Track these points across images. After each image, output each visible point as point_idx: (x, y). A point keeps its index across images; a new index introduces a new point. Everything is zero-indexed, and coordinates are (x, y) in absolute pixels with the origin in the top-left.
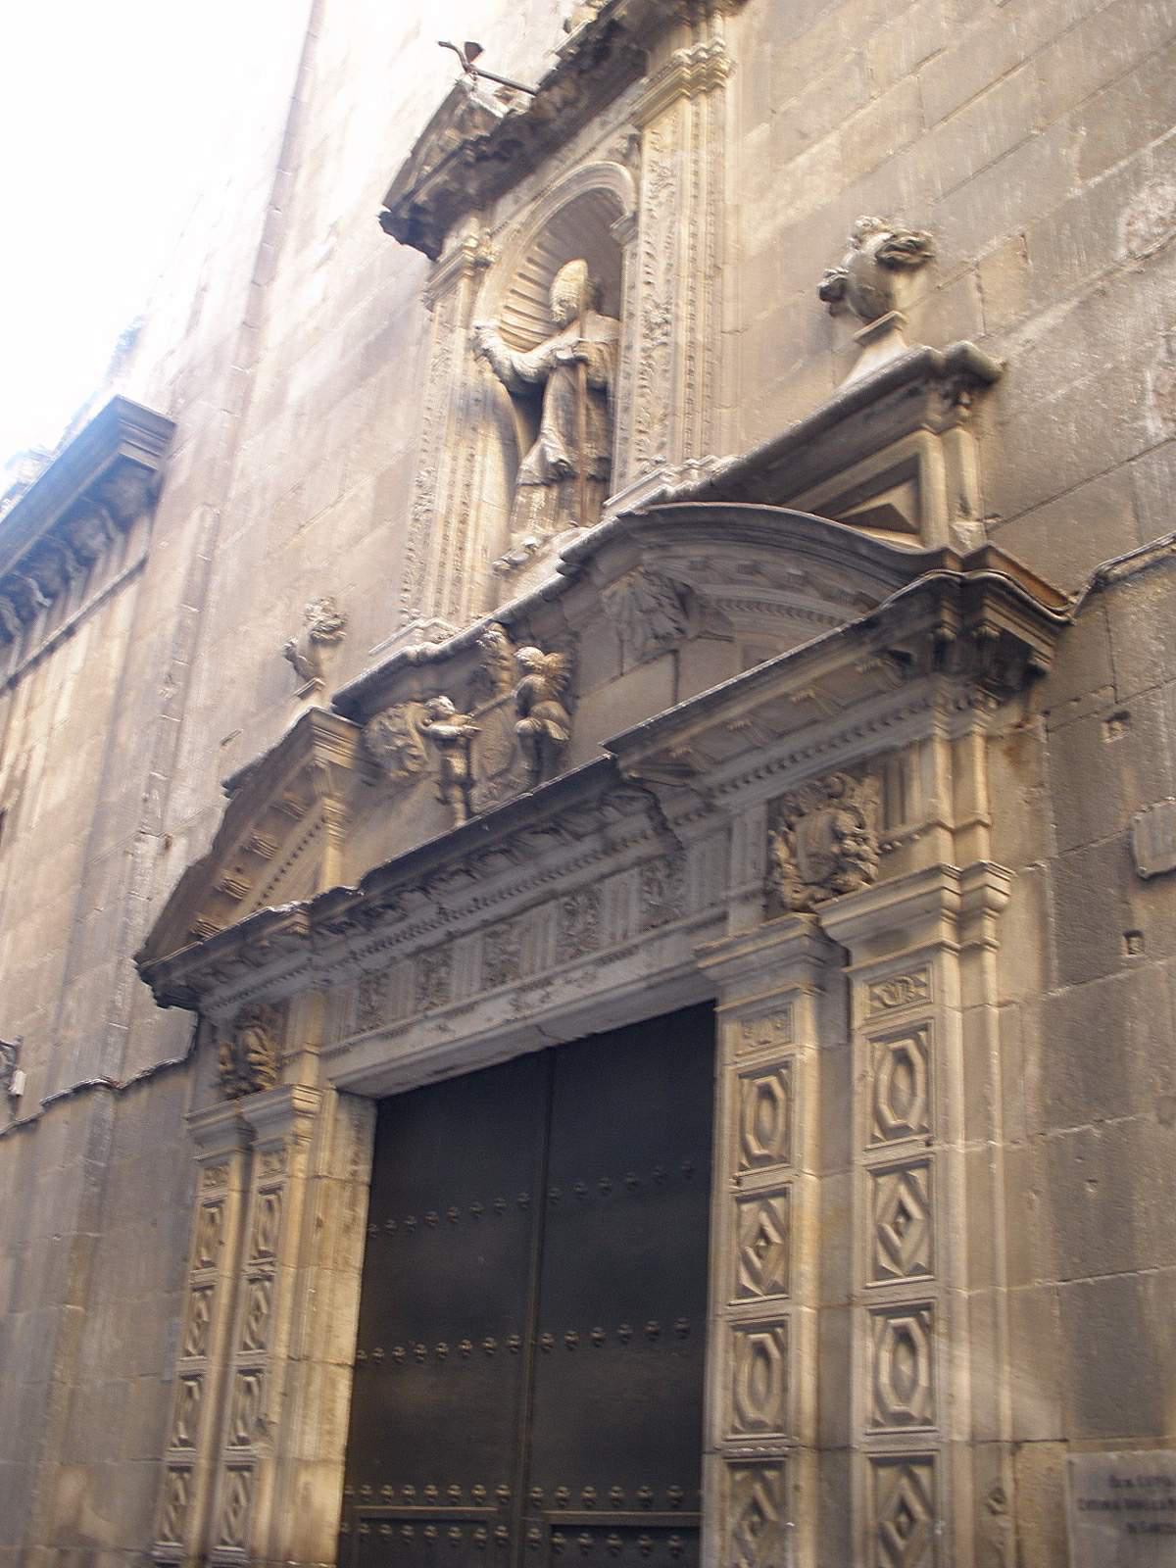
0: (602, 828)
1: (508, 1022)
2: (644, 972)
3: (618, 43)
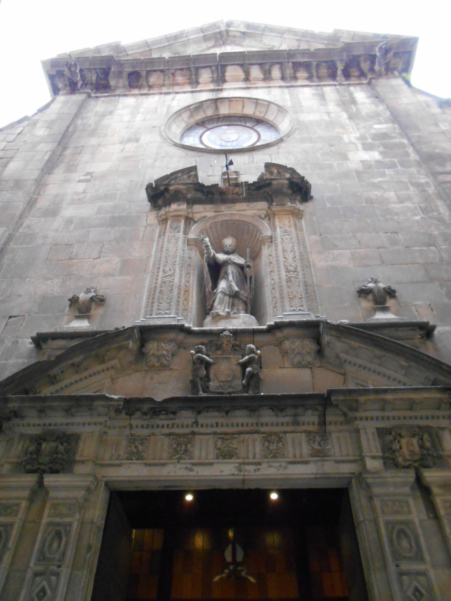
0: (296, 415)
1: (233, 474)
2: (315, 471)
3: (267, 189)
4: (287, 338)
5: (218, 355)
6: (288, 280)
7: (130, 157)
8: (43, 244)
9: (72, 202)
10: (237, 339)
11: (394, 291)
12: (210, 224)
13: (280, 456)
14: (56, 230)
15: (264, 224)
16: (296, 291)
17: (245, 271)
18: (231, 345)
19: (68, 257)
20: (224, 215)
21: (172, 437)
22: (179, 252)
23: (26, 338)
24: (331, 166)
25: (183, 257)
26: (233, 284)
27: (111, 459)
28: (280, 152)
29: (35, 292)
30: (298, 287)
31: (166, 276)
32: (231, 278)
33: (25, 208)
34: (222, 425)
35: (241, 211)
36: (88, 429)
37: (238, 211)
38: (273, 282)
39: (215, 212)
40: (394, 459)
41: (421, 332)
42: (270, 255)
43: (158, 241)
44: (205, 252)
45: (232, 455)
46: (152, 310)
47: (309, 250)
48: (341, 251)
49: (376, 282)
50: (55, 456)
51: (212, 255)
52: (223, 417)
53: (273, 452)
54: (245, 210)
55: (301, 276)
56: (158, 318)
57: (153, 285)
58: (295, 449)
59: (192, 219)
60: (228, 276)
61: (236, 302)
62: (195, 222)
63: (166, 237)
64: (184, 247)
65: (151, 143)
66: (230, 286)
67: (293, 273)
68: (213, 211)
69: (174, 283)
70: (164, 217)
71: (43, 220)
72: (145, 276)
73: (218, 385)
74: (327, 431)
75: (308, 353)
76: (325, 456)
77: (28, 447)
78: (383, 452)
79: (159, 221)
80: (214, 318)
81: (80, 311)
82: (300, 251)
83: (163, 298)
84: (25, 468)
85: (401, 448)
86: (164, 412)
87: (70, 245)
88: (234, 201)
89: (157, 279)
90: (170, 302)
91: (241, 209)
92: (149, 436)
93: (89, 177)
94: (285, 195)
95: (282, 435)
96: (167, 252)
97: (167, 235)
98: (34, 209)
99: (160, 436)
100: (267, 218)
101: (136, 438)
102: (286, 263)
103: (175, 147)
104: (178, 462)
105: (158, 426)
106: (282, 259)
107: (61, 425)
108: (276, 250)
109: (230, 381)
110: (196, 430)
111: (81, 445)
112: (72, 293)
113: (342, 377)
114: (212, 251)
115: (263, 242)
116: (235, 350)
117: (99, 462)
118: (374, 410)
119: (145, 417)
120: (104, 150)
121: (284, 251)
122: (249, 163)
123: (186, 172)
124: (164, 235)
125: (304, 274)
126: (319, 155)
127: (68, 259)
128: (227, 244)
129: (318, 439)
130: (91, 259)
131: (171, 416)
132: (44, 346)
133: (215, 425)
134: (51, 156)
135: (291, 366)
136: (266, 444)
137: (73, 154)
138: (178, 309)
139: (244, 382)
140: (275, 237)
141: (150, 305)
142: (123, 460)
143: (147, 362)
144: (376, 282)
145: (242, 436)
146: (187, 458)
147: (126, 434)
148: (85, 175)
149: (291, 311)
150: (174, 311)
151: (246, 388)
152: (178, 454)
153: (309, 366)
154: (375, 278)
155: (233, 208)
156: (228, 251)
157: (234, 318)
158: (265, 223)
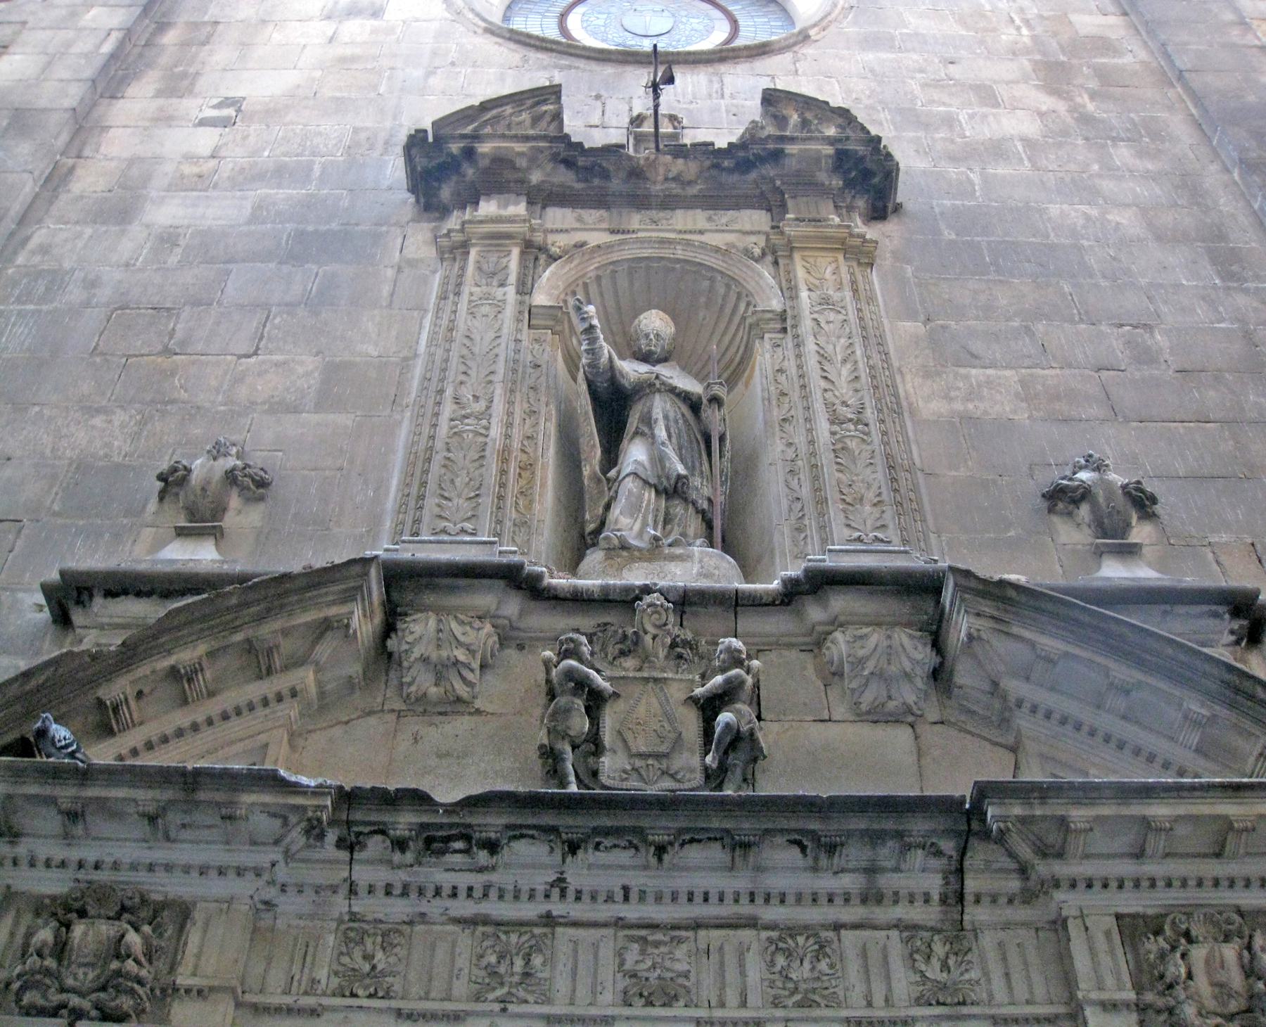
0: (872, 870)
3: (769, 170)
4: (836, 623)
5: (625, 669)
6: (839, 446)
7: (354, 59)
8: (87, 304)
9: (180, 185)
10: (685, 623)
11: (1153, 500)
12: (597, 268)
13: (823, 1003)
14: (127, 265)
15: (761, 276)
16: (863, 481)
17: (703, 415)
18: (668, 640)
19: (160, 347)
20: (638, 240)
21: (481, 929)
22: (503, 346)
23: (25, 591)
24: (949, 121)
25: (515, 361)
26: (670, 452)
27: (287, 992)
28: (800, 72)
29: (53, 450)
30: (869, 470)
31: (466, 417)
32: (661, 432)
33: (37, 196)
34: (642, 896)
35: (690, 232)
36: (218, 887)
37: (680, 232)
38: (790, 454)
39: (613, 232)
40: (1171, 1011)
41: (1236, 625)
42: (780, 371)
43: (438, 309)
44: (583, 348)
45: (673, 993)
46: (417, 521)
47: (896, 364)
48: (990, 372)
49: (1099, 467)
50: (115, 965)
51: (604, 360)
52: (646, 867)
53: (803, 986)
54: (701, 232)
55: (876, 437)
56: (439, 542)
57: (422, 446)
58: (868, 981)
59: (542, 249)
60: (651, 428)
61: (678, 509)
62: (553, 258)
63: (465, 297)
64: (519, 331)
65: (417, 20)
66: (659, 460)
67: (852, 427)
68: (605, 230)
69: (488, 440)
70: (457, 237)
71: (88, 231)
72: (398, 417)
73: (628, 767)
74: (967, 925)
75: (907, 676)
76: (964, 1003)
77: (29, 935)
78: (1139, 988)
79: (441, 253)
80: (610, 551)
81: (192, 513)
82: (871, 362)
83: (452, 481)
84: (18, 1000)
85: (1190, 976)
86: (459, 845)
87: (168, 309)
88: (669, 203)
89: (435, 425)
90: (477, 495)
91: (690, 227)
92: (411, 923)
93: (231, 112)
94: (822, 191)
95: (830, 934)
96: (466, 341)
97: (466, 290)
98: (64, 197)
99: (442, 924)
100: (769, 258)
101: (365, 926)
102: (829, 395)
103: (488, 36)
104: (504, 1010)
105: (438, 892)
106: (817, 384)
107: (134, 867)
108: (799, 356)
109: (666, 756)
110: (558, 908)
111: (194, 937)
112: (167, 458)
113: (1009, 758)
114: (606, 349)
115: (755, 330)
116: (680, 657)
117: (249, 998)
118: (1109, 856)
119: (397, 857)
120: (277, 37)
121: (823, 357)
122: (710, 96)
123: (529, 102)
124: (458, 294)
125: (885, 433)
126: (917, 90)
127: (159, 354)
128: (648, 330)
129: (939, 949)
130: (229, 358)
131: (483, 857)
132: (77, 617)
133: (619, 896)
134: (121, 44)
135: (851, 718)
136: (781, 961)
137: (185, 44)
138: (499, 522)
139: (709, 759)
140: (794, 317)
141: (412, 504)
142: (324, 994)
143: (402, 684)
144: (1099, 467)
145: (702, 933)
146: (531, 998)
147: (336, 915)
148: (219, 106)
149: (849, 541)
150: (486, 522)
151: (715, 777)
152: (502, 984)
153: (906, 717)
154: (1096, 456)
155: (664, 222)
156: (650, 353)
157: (673, 558)
158: (765, 272)
